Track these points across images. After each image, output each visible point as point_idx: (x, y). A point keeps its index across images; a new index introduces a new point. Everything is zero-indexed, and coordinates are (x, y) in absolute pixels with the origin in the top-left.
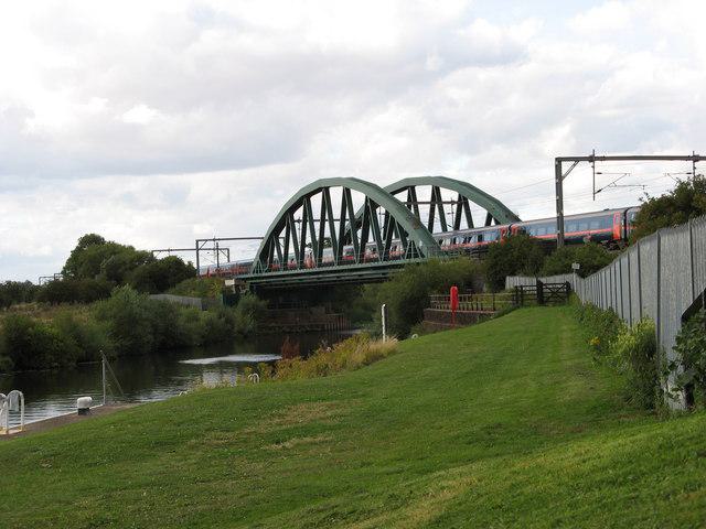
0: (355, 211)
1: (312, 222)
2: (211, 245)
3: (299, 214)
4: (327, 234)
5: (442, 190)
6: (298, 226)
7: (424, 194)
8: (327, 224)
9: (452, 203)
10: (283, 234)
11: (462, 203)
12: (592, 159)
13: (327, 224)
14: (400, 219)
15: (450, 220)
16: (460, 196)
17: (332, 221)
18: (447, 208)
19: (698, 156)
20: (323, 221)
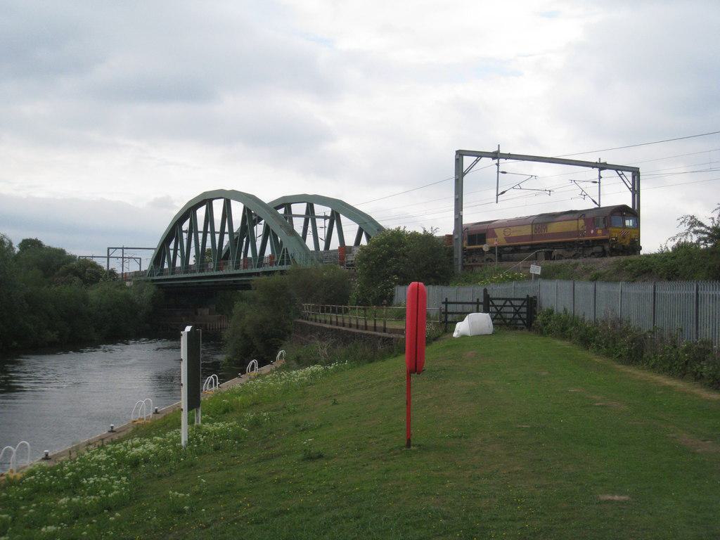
0: (235, 230)
1: (197, 233)
2: (119, 253)
3: (186, 226)
4: (209, 245)
5: (316, 207)
6: (185, 236)
7: (299, 209)
8: (209, 235)
9: (325, 218)
10: (172, 246)
11: (334, 218)
12: (496, 155)
13: (209, 235)
14: (275, 227)
15: (322, 234)
16: (332, 212)
17: (213, 233)
18: (320, 223)
19: (605, 164)
20: (205, 233)
